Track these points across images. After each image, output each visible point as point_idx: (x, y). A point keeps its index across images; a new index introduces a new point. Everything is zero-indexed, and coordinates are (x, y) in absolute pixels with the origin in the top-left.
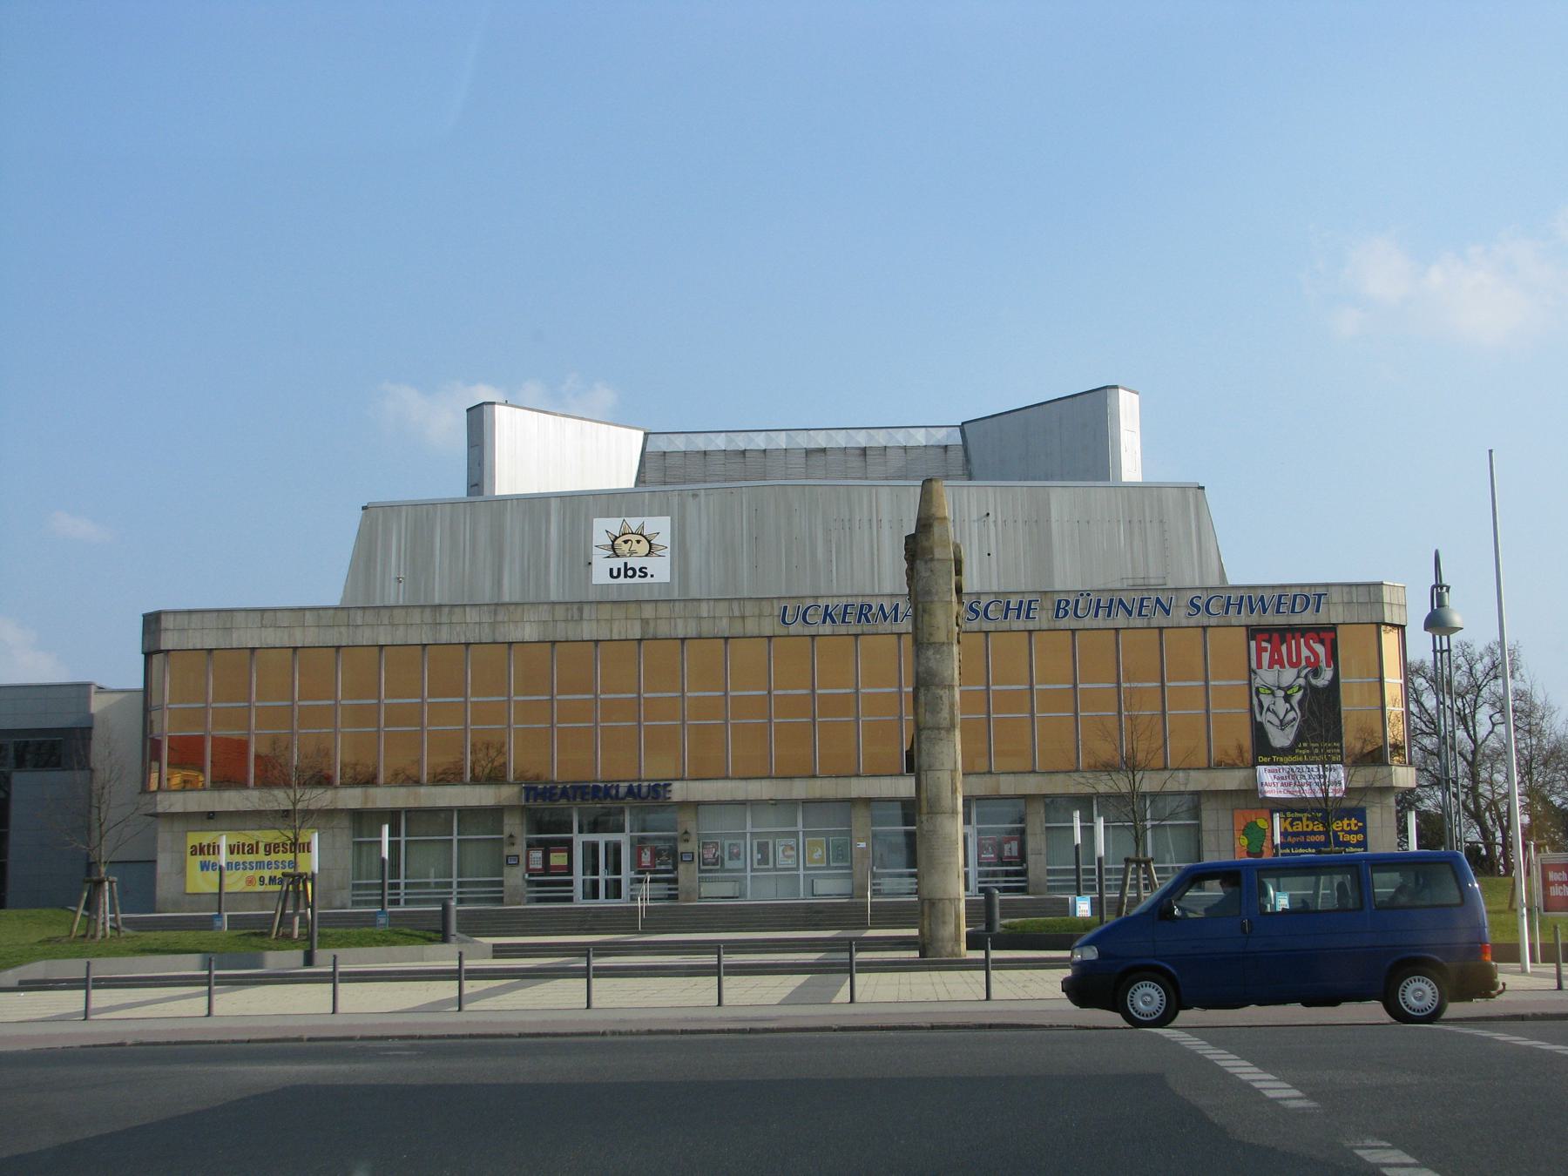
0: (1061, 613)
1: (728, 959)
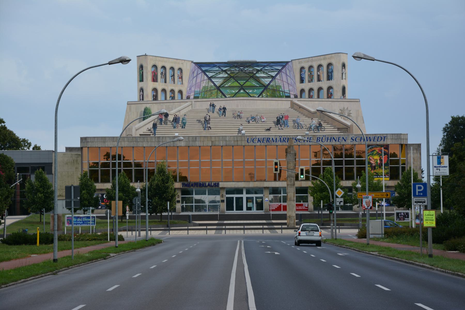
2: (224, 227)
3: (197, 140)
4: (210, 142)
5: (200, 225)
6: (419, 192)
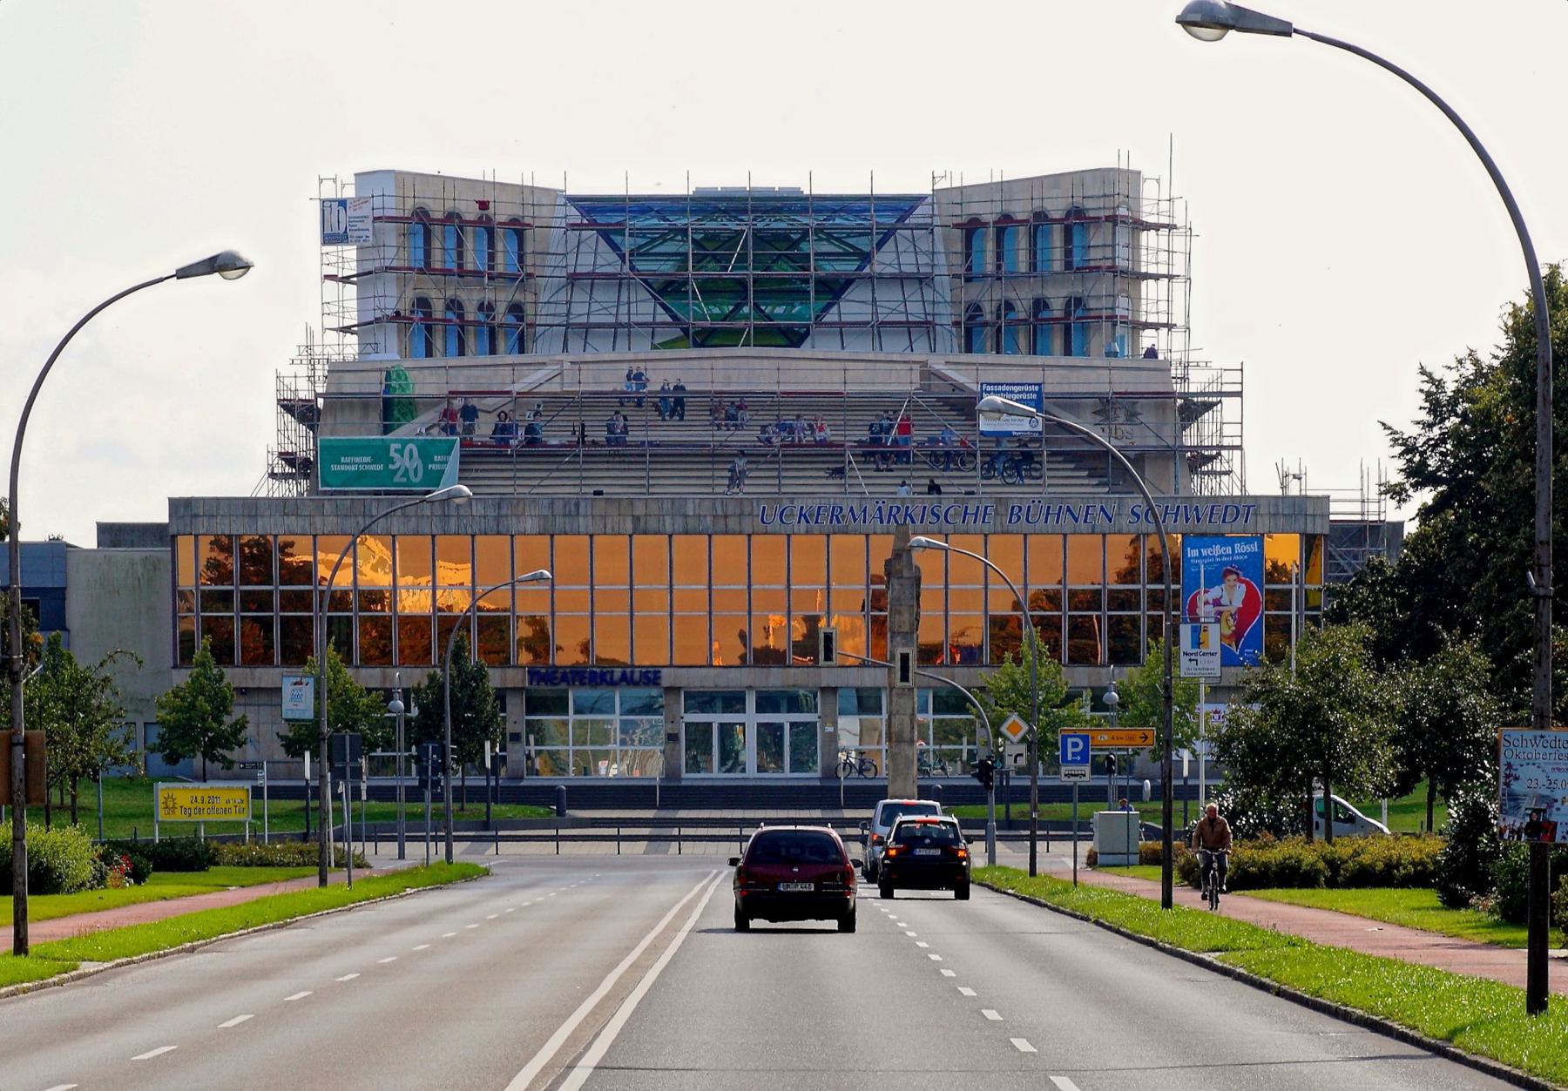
0: (1014, 519)
1: (624, 832)
2: (675, 832)
3: (582, 511)
4: (629, 521)
5: (594, 823)
6: (1074, 754)
